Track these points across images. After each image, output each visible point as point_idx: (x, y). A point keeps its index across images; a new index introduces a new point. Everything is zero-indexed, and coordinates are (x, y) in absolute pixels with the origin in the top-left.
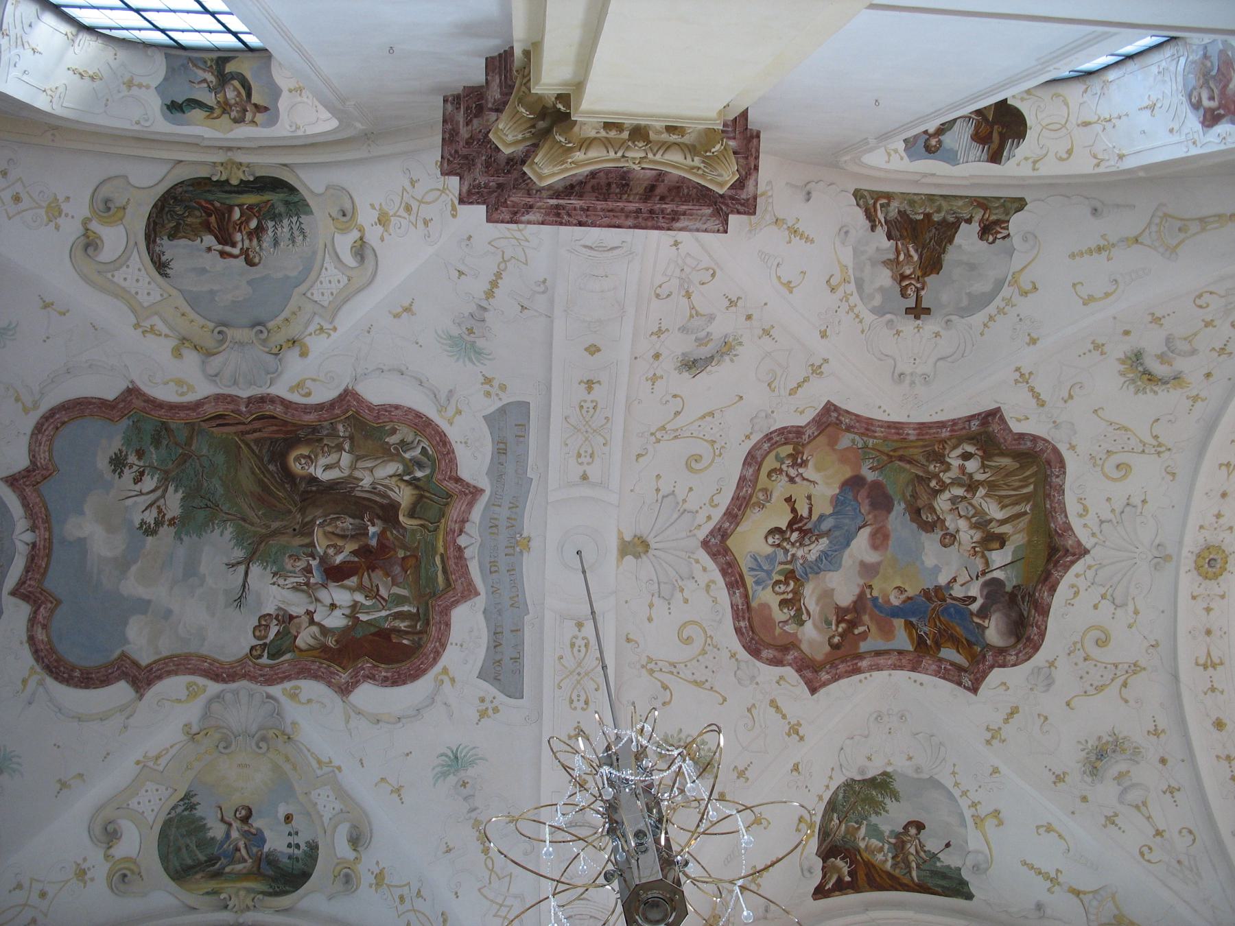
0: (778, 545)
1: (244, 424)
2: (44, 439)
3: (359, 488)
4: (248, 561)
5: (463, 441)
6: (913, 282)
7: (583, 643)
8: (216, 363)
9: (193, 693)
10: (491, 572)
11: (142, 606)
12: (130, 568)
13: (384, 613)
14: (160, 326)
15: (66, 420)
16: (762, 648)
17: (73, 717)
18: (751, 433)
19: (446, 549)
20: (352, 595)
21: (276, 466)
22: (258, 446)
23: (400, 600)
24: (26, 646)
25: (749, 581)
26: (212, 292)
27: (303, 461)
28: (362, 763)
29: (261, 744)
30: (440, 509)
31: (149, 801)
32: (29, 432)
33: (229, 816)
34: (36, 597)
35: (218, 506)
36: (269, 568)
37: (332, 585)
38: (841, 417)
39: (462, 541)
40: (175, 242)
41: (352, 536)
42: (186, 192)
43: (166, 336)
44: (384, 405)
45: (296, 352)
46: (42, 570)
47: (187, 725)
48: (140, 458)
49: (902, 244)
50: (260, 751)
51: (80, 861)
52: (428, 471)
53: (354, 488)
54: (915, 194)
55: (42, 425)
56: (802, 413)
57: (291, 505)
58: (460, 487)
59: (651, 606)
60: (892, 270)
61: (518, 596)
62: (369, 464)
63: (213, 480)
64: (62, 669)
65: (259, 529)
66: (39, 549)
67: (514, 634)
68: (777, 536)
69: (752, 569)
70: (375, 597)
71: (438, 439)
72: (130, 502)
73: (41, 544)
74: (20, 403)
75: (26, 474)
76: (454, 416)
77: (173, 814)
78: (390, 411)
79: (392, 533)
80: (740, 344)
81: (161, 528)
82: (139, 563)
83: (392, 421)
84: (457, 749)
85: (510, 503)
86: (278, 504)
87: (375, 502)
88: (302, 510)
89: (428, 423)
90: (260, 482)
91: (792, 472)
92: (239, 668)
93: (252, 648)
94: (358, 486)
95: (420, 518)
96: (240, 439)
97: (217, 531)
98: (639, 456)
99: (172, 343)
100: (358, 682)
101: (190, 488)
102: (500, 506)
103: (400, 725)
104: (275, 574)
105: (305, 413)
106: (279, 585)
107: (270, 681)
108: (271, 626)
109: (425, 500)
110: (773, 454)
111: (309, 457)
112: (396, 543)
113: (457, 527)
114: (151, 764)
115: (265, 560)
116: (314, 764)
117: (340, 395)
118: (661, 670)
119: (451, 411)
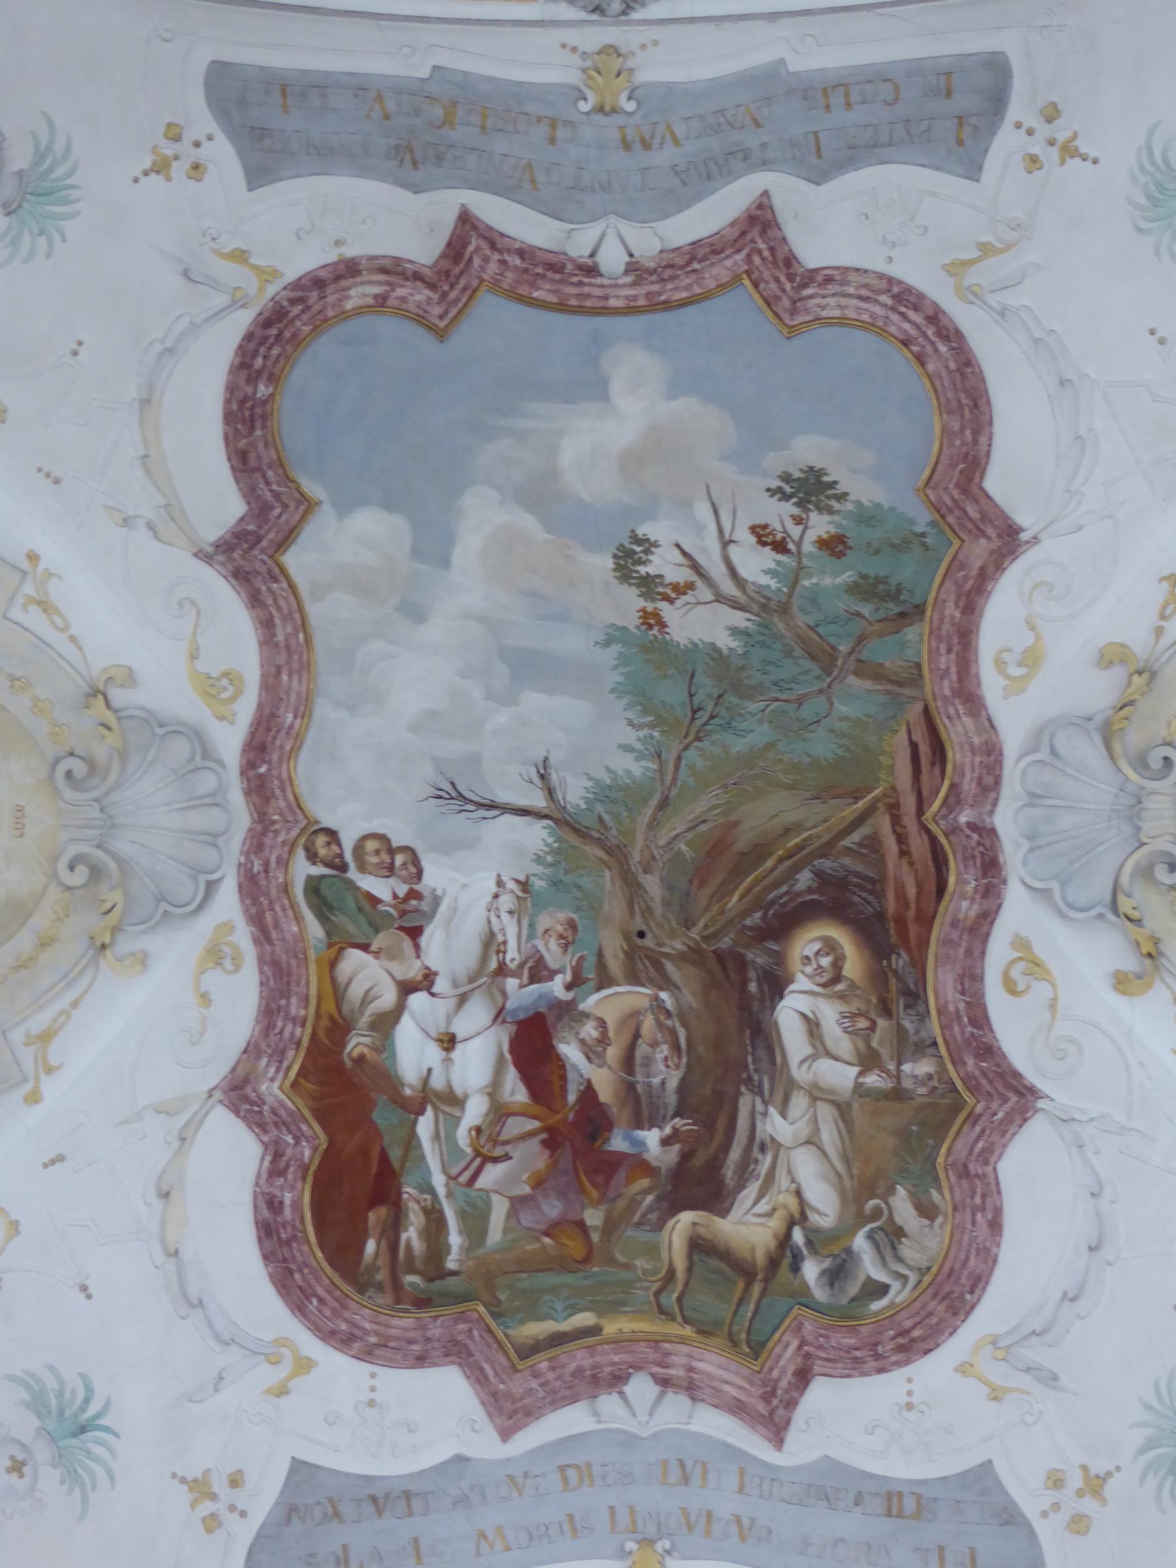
1: (920, 812)
2: (877, 309)
3: (760, 1107)
5: (915, 1400)
10: (562, 1469)
13: (439, 1181)
15: (931, 367)
17: (151, 388)
19: (617, 1342)
20: (480, 1091)
21: (810, 890)
22: (860, 844)
24: (332, 257)
27: (825, 961)
28: (53, 1162)
30: (718, 1324)
32: (895, 271)
34: (458, 277)
35: (698, 739)
36: (539, 869)
37: (502, 1036)
39: (640, 1387)
41: (631, 1087)
43: (1159, 632)
44: (999, 1192)
45: (1129, 963)
46: (523, 290)
47: (130, 678)
50: (62, 865)
52: (820, 1294)
57: (706, 926)
58: (784, 1384)
62: (829, 1135)
63: (766, 724)
64: (276, 351)
65: (640, 842)
66: (580, 284)
70: (478, 1153)
71: (916, 1333)
72: (703, 512)
74: (975, 254)
75: (780, 255)
76: (986, 1383)
78: (983, 1209)
79: (645, 1192)
81: (635, 591)
82: (543, 535)
83: (955, 1208)
86: (708, 890)
87: (726, 1147)
88: (693, 956)
90: (759, 851)
92: (282, 804)
94: (766, 1103)
95: (690, 1270)
96: (876, 800)
97: (631, 736)
99: (1139, 640)
101: (743, 668)
102: (741, 1490)
103: (160, 1258)
104: (524, 885)
105: (961, 978)
106: (496, 896)
108: (391, 881)
109: (741, 1285)
111: (837, 979)
112: (621, 1204)
113: (677, 1372)
114: (29, 589)
116: (39, 1022)
117: (1016, 1075)
119: (997, 1373)
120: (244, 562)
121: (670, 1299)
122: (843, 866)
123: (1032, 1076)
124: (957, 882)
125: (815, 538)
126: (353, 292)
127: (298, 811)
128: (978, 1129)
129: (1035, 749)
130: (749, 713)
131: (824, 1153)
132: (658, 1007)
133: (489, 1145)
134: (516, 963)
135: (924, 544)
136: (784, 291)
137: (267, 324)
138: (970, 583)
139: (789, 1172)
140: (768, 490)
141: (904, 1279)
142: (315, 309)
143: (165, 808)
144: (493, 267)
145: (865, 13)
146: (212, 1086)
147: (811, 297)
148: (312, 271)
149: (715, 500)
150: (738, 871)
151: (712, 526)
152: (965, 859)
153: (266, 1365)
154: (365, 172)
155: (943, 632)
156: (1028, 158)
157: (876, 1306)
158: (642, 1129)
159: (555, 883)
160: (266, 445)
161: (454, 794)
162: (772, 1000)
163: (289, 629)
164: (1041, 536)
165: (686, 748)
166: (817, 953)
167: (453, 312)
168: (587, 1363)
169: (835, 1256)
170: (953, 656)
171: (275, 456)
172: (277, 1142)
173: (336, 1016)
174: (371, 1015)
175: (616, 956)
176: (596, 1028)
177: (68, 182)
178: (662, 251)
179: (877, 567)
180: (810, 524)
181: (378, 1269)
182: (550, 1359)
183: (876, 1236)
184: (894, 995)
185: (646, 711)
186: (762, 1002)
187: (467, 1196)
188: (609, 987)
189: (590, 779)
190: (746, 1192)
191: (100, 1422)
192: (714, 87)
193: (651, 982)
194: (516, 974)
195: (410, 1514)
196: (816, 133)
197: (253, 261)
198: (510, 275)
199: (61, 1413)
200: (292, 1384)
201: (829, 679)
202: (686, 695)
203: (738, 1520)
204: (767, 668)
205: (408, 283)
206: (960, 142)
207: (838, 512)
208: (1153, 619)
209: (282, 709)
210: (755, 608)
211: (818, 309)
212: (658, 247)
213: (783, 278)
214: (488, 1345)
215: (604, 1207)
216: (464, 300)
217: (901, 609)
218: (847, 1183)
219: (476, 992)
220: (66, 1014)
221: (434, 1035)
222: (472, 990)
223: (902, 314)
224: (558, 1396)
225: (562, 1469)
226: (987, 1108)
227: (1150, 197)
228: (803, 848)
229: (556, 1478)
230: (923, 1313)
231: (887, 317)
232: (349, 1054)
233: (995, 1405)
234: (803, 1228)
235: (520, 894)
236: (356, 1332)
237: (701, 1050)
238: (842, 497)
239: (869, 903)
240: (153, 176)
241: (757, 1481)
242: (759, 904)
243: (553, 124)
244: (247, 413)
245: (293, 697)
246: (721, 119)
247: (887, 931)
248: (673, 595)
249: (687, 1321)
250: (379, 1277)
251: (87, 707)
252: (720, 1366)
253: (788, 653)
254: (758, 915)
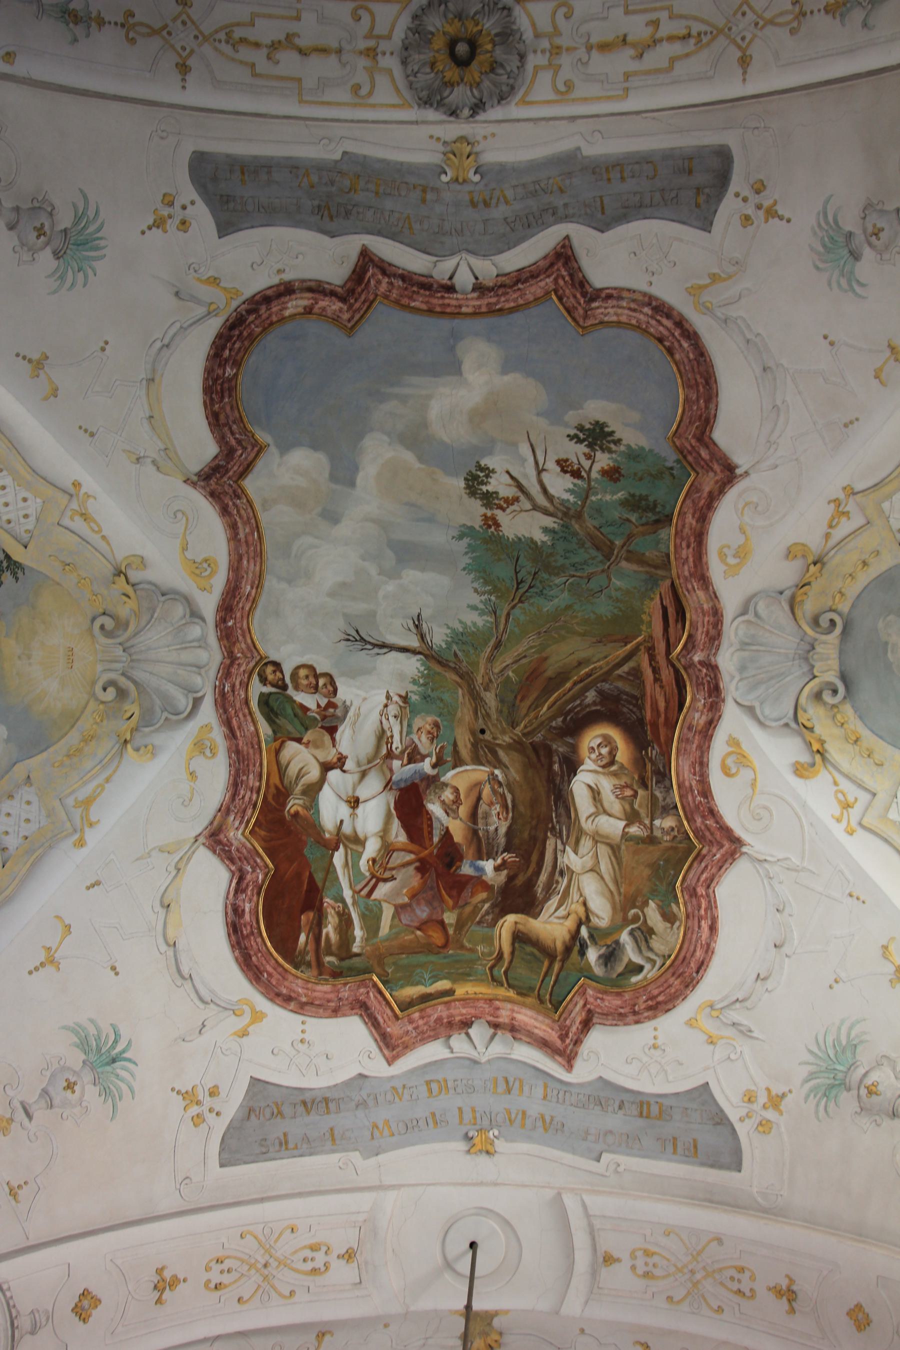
1: (668, 652)
2: (642, 317)
3: (560, 847)
4: (428, 654)
5: (659, 1042)
7: (319, 1263)
8: (781, 614)
10: (428, 1083)
12: (408, 448)
13: (347, 894)
14: (845, 527)
15: (677, 357)
17: (154, 370)
19: (464, 1000)
20: (376, 834)
21: (594, 703)
22: (628, 673)
23: (372, 920)
24: (275, 280)
27: (604, 751)
28: (93, 886)
29: (111, 691)
30: (532, 989)
32: (655, 291)
34: (360, 295)
35: (520, 601)
36: (415, 688)
37: (390, 798)
39: (478, 1031)
41: (475, 832)
43: (827, 536)
46: (405, 301)
47: (143, 563)
48: (604, 473)
52: (598, 971)
53: (561, 837)
55: (668, 316)
57: (525, 727)
61: (393, 1135)
62: (605, 866)
63: (566, 593)
64: (237, 346)
65: (482, 671)
66: (443, 297)
67: (328, 1135)
70: (373, 876)
71: (660, 998)
72: (525, 450)
73: (452, 300)
74: (708, 281)
81: (479, 502)
82: (418, 465)
83: (688, 917)
84: (130, 1060)
85: (552, 1118)
86: (528, 702)
88: (517, 746)
89: (690, 984)
90: (562, 677)
92: (243, 646)
93: (277, 665)
94: (564, 844)
95: (513, 953)
97: (476, 600)
100: (232, 860)
101: (551, 555)
103: (163, 948)
104: (405, 699)
105: (693, 765)
106: (386, 706)
107: (223, 702)
108: (317, 696)
109: (546, 963)
111: (612, 762)
112: (468, 909)
114: (74, 505)
115: (428, 681)
116: (83, 794)
119: (708, 1025)
120: (217, 487)
121: (500, 971)
122: (617, 687)
123: (739, 832)
124: (692, 700)
125: (600, 468)
126: (289, 305)
127: (254, 650)
128: (703, 865)
129: (744, 612)
130: (556, 585)
131: (602, 878)
132: (494, 779)
133: (382, 870)
134: (399, 750)
135: (672, 475)
136: (580, 304)
137: (232, 327)
138: (702, 502)
139: (579, 889)
140: (568, 436)
141: (654, 963)
142: (264, 317)
143: (167, 649)
144: (384, 287)
145: (634, 116)
146: (198, 833)
147: (598, 308)
148: (262, 291)
149: (533, 443)
150: (547, 691)
151: (531, 460)
152: (698, 685)
153: (233, 1017)
154: (297, 224)
155: (684, 534)
156: (743, 217)
157: (634, 979)
158: (483, 860)
159: (425, 697)
160: (232, 408)
161: (358, 638)
162: (569, 776)
163: (247, 530)
164: (750, 472)
165: (513, 607)
166: (599, 745)
167: (357, 317)
168: (445, 1014)
169: (608, 946)
170: (691, 550)
171: (238, 415)
172: (241, 870)
173: (280, 786)
174: (303, 785)
175: (466, 746)
176: (452, 794)
177: (98, 235)
178: (497, 276)
179: (640, 490)
180: (596, 459)
181: (307, 953)
182: (421, 1010)
183: (636, 934)
184: (649, 774)
185: (486, 583)
186: (562, 777)
187: (367, 904)
188: (461, 766)
189: (448, 628)
190: (550, 902)
191: (125, 1055)
192: (534, 166)
193: (489, 763)
194: (399, 757)
195: (328, 1113)
196: (601, 197)
197: (222, 284)
198: (395, 291)
199: (99, 1049)
200: (250, 1029)
201: (608, 564)
202: (513, 572)
203: (543, 1117)
204: (567, 555)
205: (327, 298)
206: (698, 206)
207: (615, 452)
208: (824, 528)
209: (243, 583)
210: (560, 515)
211: (602, 316)
212: (495, 272)
213: (578, 296)
214: (379, 1002)
215: (456, 911)
216: (365, 308)
217: (657, 517)
218: (617, 897)
219: (373, 770)
220: (101, 787)
221: (345, 798)
222: (370, 768)
223: (658, 321)
224: (426, 1035)
225: (428, 1083)
226: (709, 851)
227: (824, 246)
228: (590, 675)
229: (424, 1088)
230: (666, 985)
231: (648, 323)
232: (288, 811)
233: (711, 1047)
234: (588, 927)
235: (402, 704)
236: (293, 995)
237: (522, 809)
238: (618, 442)
239: (634, 713)
240: (154, 229)
241: (555, 1092)
242: (561, 712)
243: (424, 191)
244: (219, 388)
245: (250, 575)
246: (537, 187)
247: (646, 732)
248: (505, 506)
249: (510, 986)
250: (308, 958)
251: (114, 583)
252: (531, 1017)
253: (582, 545)
254: (561, 719)
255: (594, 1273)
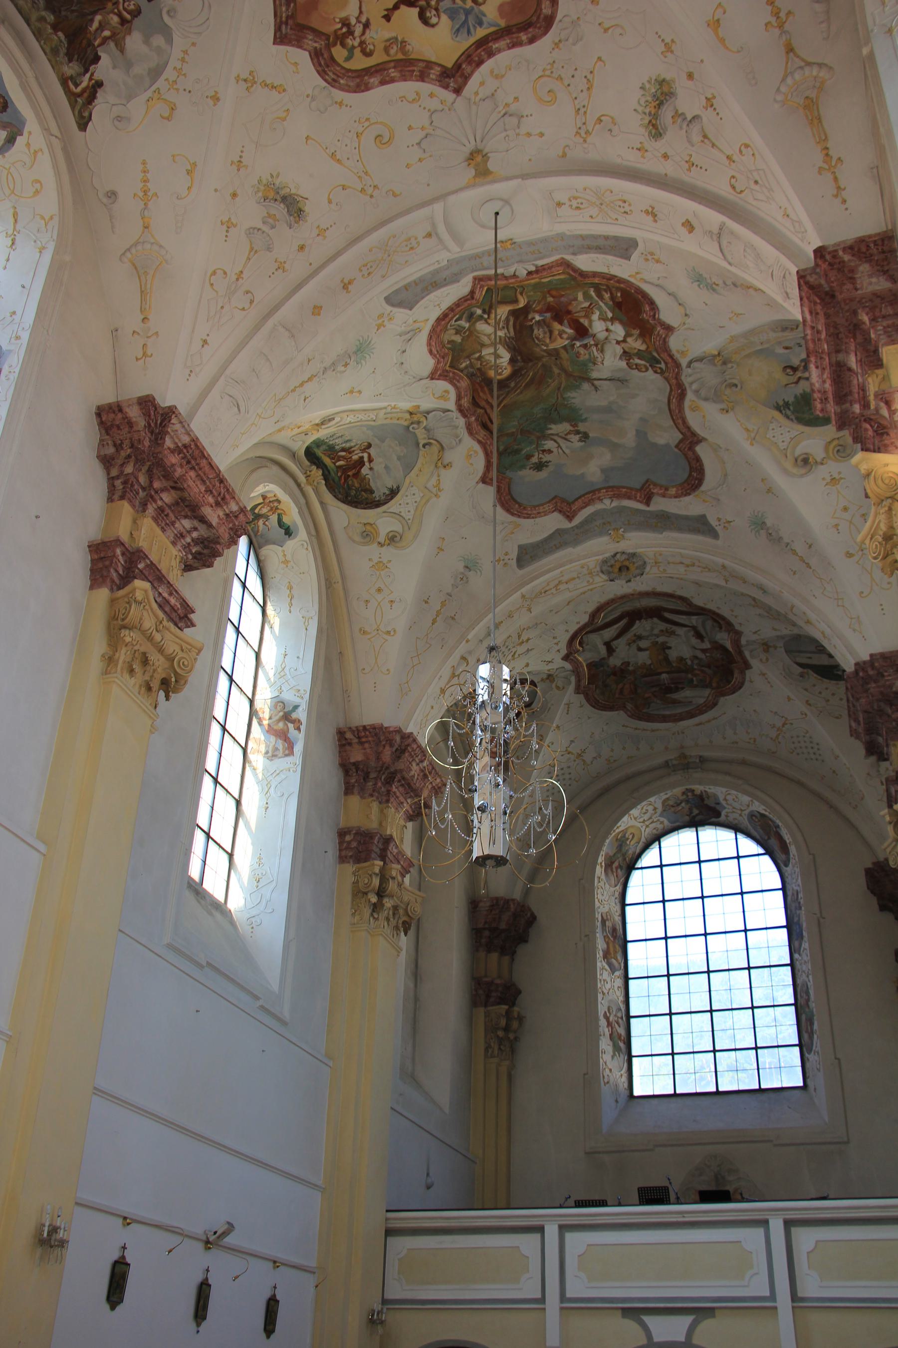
0: (437, 10)
2: (535, 512)
3: (508, 335)
4: (589, 380)
6: (121, 8)
8: (445, 442)
9: (694, 409)
11: (641, 434)
16: (542, 16)
18: (336, 103)
25: (481, 33)
26: (399, 458)
31: (782, 434)
32: (533, 520)
33: (795, 379)
38: (284, 19)
40: (374, 488)
42: (340, 492)
43: (439, 476)
46: (629, 491)
48: (533, 456)
49: (95, 39)
51: (825, 482)
54: (45, 53)
56: (296, 64)
59: (529, 135)
60: (124, 38)
68: (428, 14)
69: (469, 32)
72: (567, 451)
77: (793, 417)
80: (260, 181)
88: (539, 359)
90: (528, 386)
91: (358, 30)
97: (573, 401)
98: (395, 195)
99: (443, 472)
104: (595, 364)
110: (347, 65)
118: (584, 124)
150: (532, 381)
227: (477, 563)
238: (530, 469)
255: (434, 225)
